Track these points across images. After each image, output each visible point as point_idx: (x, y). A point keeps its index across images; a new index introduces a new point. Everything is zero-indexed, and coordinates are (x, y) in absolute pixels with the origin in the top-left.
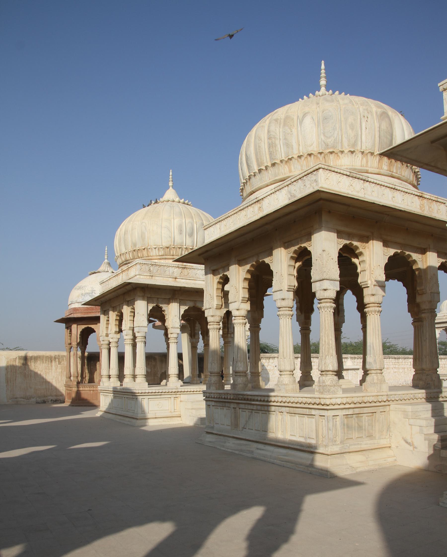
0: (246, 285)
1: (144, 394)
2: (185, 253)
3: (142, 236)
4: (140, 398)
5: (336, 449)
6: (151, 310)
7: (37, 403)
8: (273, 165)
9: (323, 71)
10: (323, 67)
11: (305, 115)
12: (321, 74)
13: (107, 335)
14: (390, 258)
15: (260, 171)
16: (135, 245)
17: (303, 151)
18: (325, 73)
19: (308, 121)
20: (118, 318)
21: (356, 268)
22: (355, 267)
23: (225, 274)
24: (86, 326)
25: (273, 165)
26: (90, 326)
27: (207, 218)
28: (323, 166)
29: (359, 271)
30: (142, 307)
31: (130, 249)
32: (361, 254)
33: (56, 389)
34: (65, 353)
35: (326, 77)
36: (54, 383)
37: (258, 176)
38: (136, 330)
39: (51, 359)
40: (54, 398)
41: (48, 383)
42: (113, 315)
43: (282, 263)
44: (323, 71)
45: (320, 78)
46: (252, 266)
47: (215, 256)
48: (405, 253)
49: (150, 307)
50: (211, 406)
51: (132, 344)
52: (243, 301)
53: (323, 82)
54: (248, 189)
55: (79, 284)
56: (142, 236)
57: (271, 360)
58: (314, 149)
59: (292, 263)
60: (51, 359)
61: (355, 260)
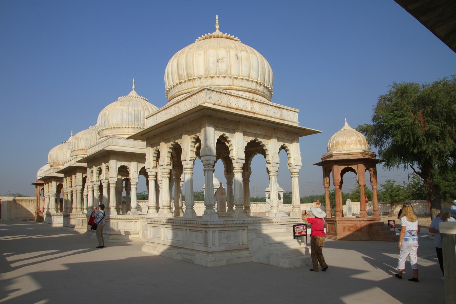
0: (170, 155)
1: (54, 215)
2: (58, 170)
3: (56, 157)
4: (52, 217)
5: (79, 227)
6: (119, 168)
7: (23, 220)
8: (181, 83)
9: (217, 20)
10: (217, 18)
11: (82, 138)
12: (216, 22)
13: (92, 182)
14: (248, 144)
15: (174, 86)
16: (54, 160)
17: (80, 148)
18: (218, 22)
19: (82, 140)
20: (98, 172)
21: (228, 148)
22: (227, 148)
23: (176, 141)
24: (346, 167)
25: (181, 83)
26: (350, 166)
27: (153, 108)
28: (207, 88)
29: (229, 150)
30: (114, 165)
31: (52, 161)
32: (230, 141)
33: (32, 214)
34: (35, 198)
35: (219, 24)
36: (31, 211)
37: (173, 89)
38: (109, 179)
39: (29, 201)
40: (31, 218)
41: (29, 211)
42: (95, 169)
43: (187, 144)
44: (217, 20)
45: (215, 24)
46: (172, 145)
47: (152, 136)
48: (258, 140)
49: (58, 184)
50: (188, 230)
51: (169, 177)
52: (168, 165)
53: (217, 27)
54: (170, 95)
55: (41, 169)
56: (56, 157)
57: (144, 203)
58: (84, 148)
59: (193, 144)
60: (29, 201)
61: (227, 144)
